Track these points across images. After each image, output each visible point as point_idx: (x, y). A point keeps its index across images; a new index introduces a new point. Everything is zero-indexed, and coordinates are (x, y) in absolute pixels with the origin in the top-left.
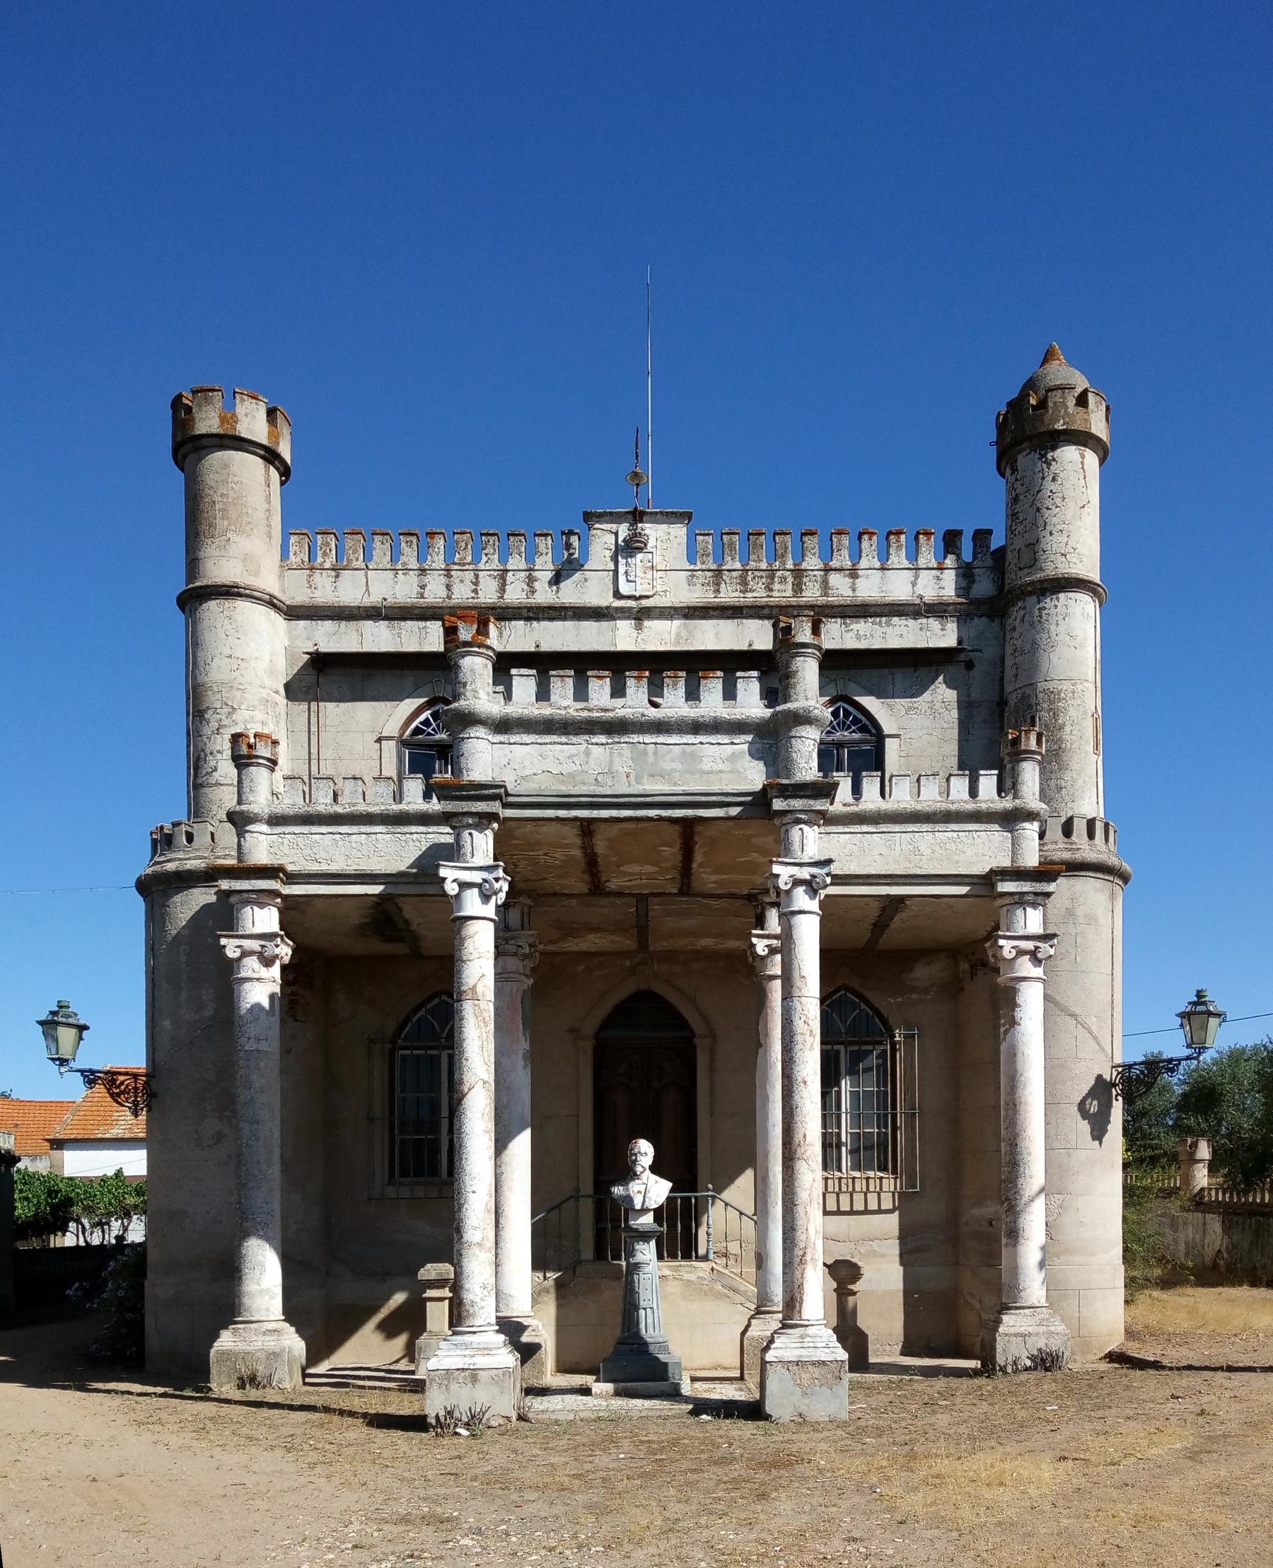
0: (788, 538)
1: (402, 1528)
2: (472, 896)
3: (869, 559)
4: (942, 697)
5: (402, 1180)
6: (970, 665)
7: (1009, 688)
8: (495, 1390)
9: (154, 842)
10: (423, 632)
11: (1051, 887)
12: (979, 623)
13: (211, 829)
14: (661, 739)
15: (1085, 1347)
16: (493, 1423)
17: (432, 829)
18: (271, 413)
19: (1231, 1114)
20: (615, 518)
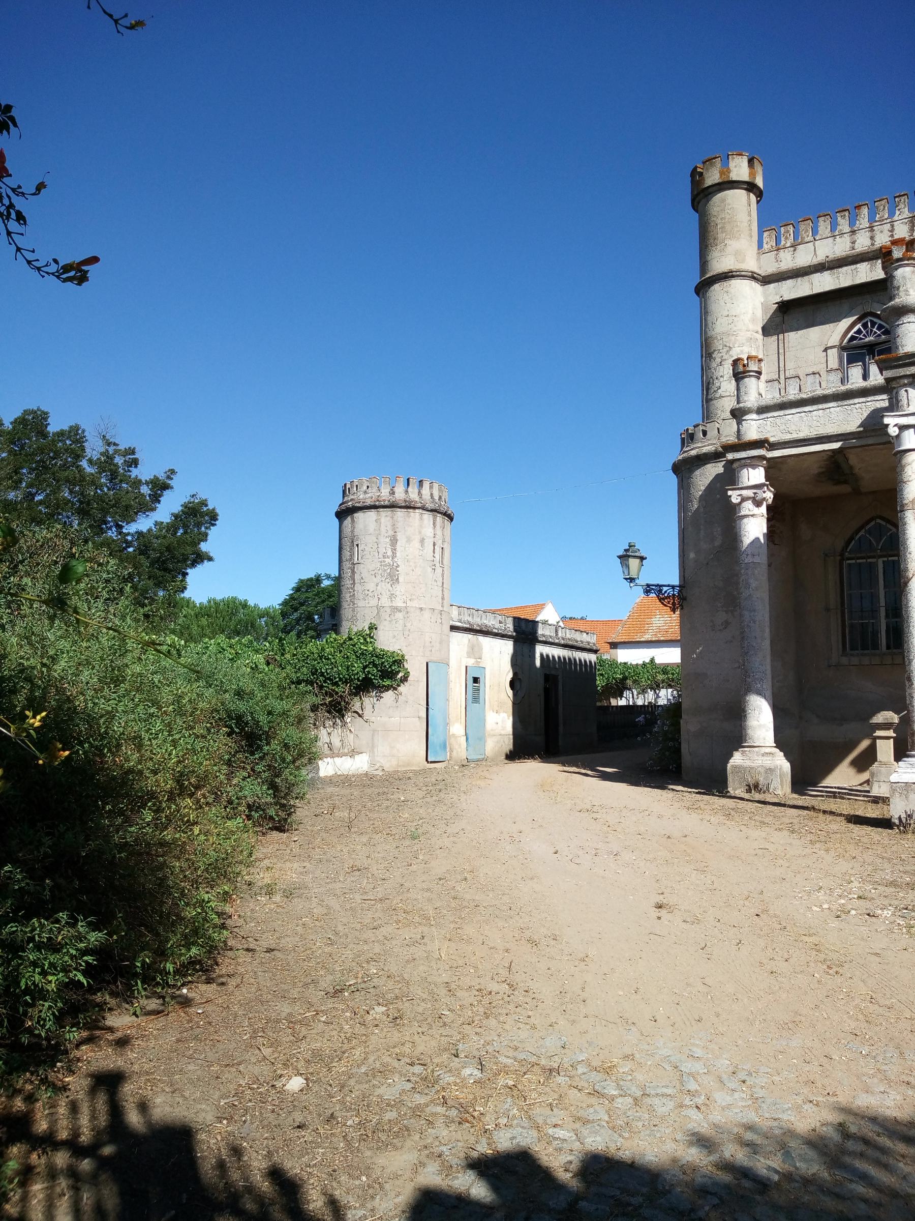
1: (893, 889)
5: (852, 652)
9: (683, 440)
10: (855, 272)
13: (717, 425)
17: (870, 399)
18: (751, 161)
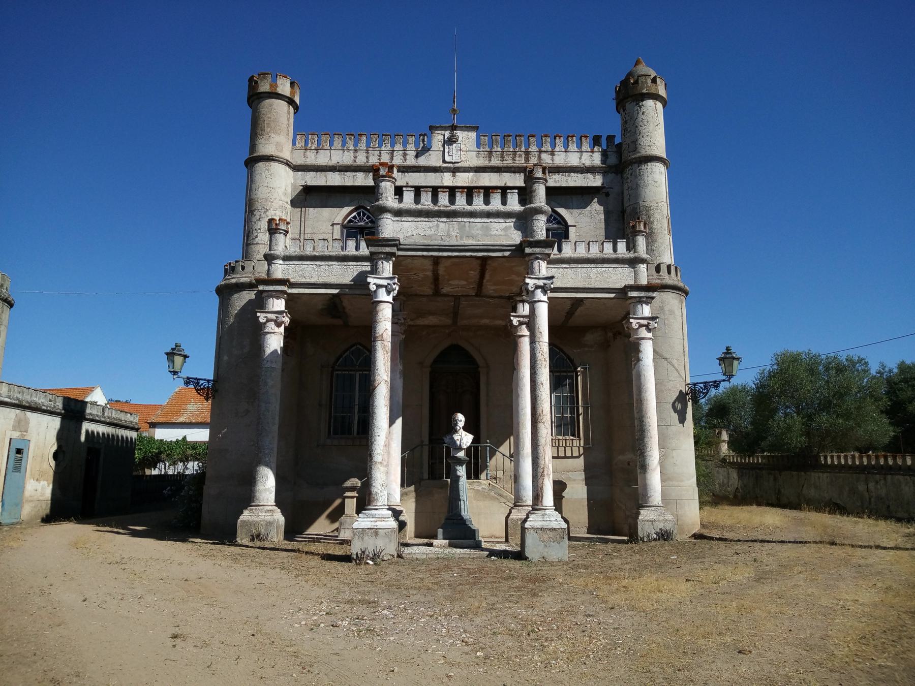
0: (522, 138)
1: (349, 606)
2: (382, 291)
3: (559, 147)
4: (596, 208)
6: (607, 195)
7: (626, 204)
8: (387, 540)
9: (226, 270)
11: (655, 294)
12: (611, 176)
14: (472, 220)
15: (681, 531)
16: (385, 558)
18: (292, 84)
19: (735, 419)
20: (444, 128)
